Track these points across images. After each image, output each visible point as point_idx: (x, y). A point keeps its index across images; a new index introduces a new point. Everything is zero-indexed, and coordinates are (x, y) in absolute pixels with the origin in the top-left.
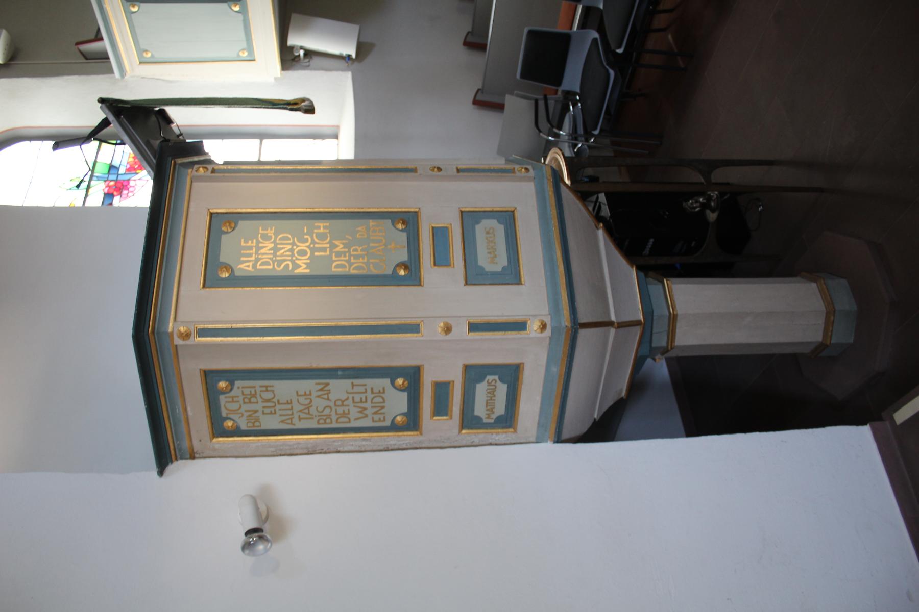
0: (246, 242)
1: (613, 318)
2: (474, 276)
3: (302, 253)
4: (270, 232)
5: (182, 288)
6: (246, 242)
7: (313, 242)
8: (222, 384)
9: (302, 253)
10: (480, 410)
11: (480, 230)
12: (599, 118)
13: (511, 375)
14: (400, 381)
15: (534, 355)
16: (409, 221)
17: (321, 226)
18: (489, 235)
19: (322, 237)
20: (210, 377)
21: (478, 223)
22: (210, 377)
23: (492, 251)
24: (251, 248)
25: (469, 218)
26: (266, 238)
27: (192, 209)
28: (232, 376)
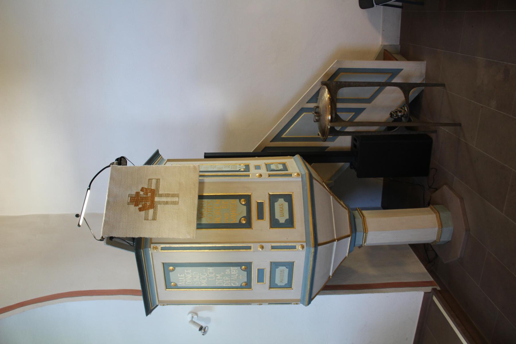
0: (180, 275)
1: (335, 238)
2: (274, 224)
3: (204, 279)
4: (190, 271)
5: (158, 290)
6: (180, 275)
7: (208, 275)
8: (171, 268)
9: (204, 279)
10: (278, 281)
11: (278, 271)
12: (334, 232)
13: (290, 265)
14: (243, 267)
15: (299, 257)
16: (247, 267)
17: (210, 269)
18: (281, 205)
19: (210, 273)
20: (165, 265)
21: (277, 268)
22: (165, 265)
23: (282, 211)
24: (182, 277)
25: (274, 265)
26: (188, 273)
27: (155, 263)
28: (176, 265)
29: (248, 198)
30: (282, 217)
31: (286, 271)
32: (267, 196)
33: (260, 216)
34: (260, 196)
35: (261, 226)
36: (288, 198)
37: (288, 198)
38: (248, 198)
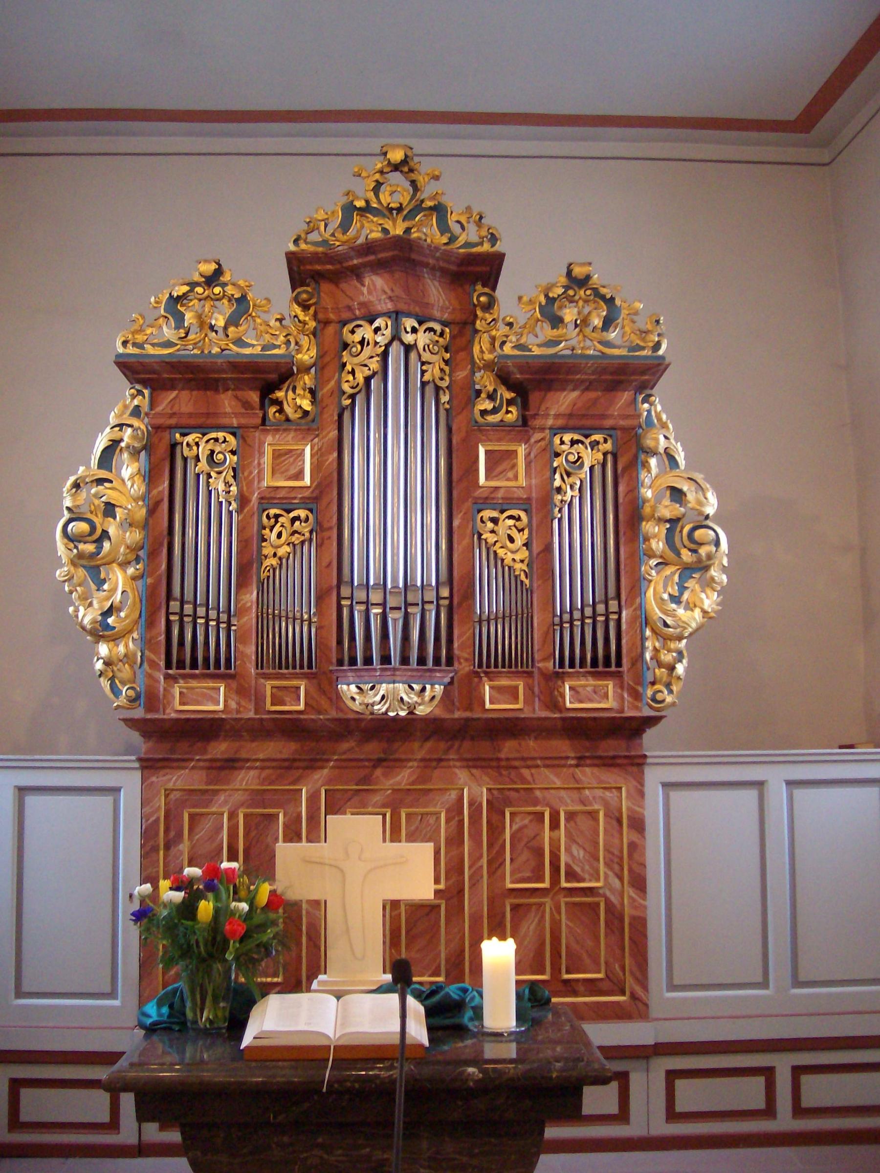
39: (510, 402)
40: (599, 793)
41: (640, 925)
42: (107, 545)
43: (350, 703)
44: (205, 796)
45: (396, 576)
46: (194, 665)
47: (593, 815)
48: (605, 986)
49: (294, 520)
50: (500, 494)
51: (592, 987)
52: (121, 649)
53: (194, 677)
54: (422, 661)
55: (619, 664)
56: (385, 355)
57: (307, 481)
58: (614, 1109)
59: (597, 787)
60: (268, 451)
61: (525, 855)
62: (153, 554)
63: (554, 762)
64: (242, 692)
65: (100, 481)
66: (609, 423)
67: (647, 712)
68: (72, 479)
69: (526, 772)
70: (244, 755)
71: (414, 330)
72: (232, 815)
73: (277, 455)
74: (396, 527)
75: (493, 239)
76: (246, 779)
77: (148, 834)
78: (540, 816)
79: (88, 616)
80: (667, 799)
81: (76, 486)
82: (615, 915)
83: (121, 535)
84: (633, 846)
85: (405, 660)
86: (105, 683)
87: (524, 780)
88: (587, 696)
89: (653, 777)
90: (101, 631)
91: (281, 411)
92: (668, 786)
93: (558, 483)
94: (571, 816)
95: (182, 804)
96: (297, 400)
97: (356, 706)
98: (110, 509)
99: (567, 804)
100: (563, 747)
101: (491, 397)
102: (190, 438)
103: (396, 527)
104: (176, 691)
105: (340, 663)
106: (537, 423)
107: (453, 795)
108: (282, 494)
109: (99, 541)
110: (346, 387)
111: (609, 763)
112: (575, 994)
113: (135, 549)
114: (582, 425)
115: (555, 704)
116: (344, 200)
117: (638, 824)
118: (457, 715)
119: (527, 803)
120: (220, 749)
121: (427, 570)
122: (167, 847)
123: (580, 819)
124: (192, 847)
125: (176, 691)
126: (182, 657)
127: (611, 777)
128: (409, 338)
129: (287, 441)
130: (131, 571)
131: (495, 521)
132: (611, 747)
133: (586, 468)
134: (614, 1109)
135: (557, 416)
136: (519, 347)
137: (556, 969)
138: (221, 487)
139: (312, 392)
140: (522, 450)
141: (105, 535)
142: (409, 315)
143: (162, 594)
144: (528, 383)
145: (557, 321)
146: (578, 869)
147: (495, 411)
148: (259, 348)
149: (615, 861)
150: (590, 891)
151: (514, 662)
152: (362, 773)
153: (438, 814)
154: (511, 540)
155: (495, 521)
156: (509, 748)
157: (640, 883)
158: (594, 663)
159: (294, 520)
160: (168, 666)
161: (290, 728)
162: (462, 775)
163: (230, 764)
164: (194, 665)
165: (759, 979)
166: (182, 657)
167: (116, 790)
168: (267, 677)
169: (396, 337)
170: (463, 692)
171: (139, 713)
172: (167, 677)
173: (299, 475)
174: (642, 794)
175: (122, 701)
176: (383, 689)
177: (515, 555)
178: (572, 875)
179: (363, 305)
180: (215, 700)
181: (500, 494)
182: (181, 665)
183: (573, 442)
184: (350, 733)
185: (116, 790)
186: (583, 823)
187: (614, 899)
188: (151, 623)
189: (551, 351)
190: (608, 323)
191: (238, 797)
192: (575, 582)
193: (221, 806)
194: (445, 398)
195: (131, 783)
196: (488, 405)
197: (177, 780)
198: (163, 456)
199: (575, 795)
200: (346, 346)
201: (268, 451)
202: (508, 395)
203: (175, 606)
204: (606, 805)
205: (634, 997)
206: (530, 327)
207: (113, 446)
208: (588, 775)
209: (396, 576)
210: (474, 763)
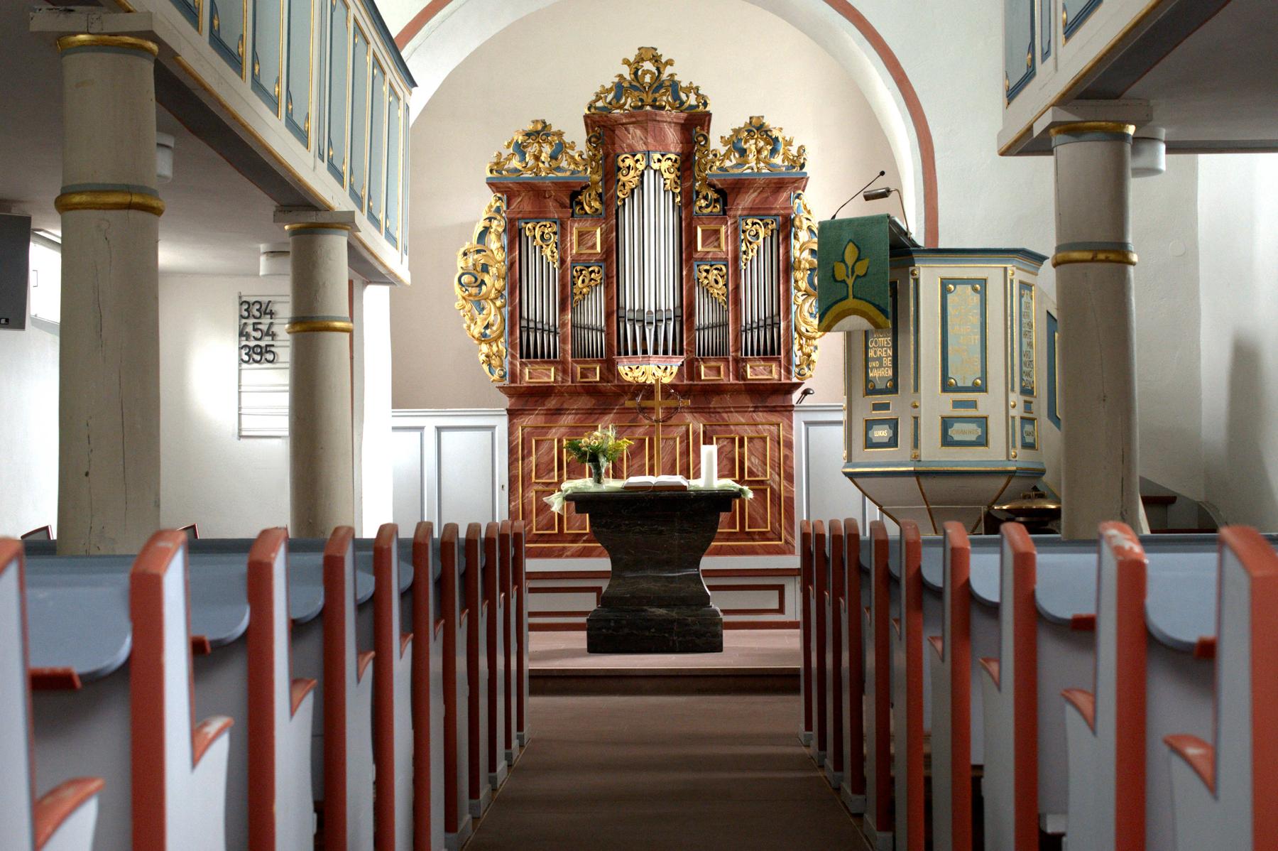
18: (881, 433)
23: (964, 432)
29: (894, 389)
30: (957, 432)
31: (973, 438)
32: (984, 414)
33: (973, 404)
34: (897, 406)
35: (865, 409)
36: (983, 441)
37: (983, 441)
38: (894, 389)
39: (716, 201)
40: (767, 427)
41: (790, 501)
42: (484, 288)
43: (625, 377)
44: (545, 429)
45: (650, 306)
46: (536, 356)
47: (764, 439)
48: (770, 536)
49: (591, 272)
50: (710, 256)
51: (763, 536)
52: (495, 349)
53: (537, 363)
54: (665, 352)
55: (779, 353)
56: (642, 175)
57: (599, 249)
58: (776, 606)
59: (765, 423)
60: (575, 231)
61: (725, 462)
62: (512, 293)
63: (741, 410)
64: (565, 372)
65: (478, 252)
66: (774, 212)
67: (795, 380)
68: (462, 250)
69: (725, 415)
70: (565, 406)
71: (659, 161)
72: (560, 441)
73: (581, 235)
74: (652, 281)
75: (705, 104)
76: (568, 420)
77: (512, 451)
78: (734, 439)
79: (477, 330)
80: (807, 431)
81: (465, 254)
82: (776, 497)
83: (492, 282)
84: (786, 457)
85: (656, 352)
86: (485, 367)
87: (723, 419)
88: (757, 372)
89: (798, 419)
90: (483, 338)
91: (583, 208)
92: (808, 424)
93: (744, 248)
94: (751, 439)
95: (531, 434)
96: (591, 204)
97: (629, 378)
98: (485, 268)
99: (748, 432)
100: (746, 401)
101: (705, 198)
102: (530, 225)
103: (652, 281)
104: (527, 371)
105: (619, 354)
106: (732, 213)
107: (684, 428)
108: (584, 257)
109: (480, 286)
110: (620, 194)
111: (773, 410)
112: (754, 540)
113: (500, 293)
114: (757, 212)
115: (740, 375)
116: (617, 80)
117: (789, 445)
118: (685, 382)
119: (726, 432)
120: (552, 403)
121: (668, 301)
122: (523, 459)
123: (756, 441)
124: (537, 459)
125: (527, 371)
126: (528, 353)
127: (774, 418)
128: (656, 166)
129: (586, 225)
130: (498, 303)
131: (707, 271)
132: (776, 401)
133: (761, 239)
134: (776, 606)
135: (743, 209)
136: (721, 169)
137: (742, 526)
138: (549, 253)
139: (600, 195)
140: (723, 229)
141: (483, 282)
142: (655, 151)
143: (515, 318)
144: (727, 192)
145: (743, 152)
146: (545, 522)
147: (707, 206)
148: (568, 173)
149: (776, 466)
150: (762, 482)
151: (719, 352)
152: (632, 416)
153: (675, 439)
154: (717, 282)
155: (707, 271)
156: (714, 403)
157: (790, 478)
158: (765, 353)
159: (591, 272)
160: (521, 357)
161: (591, 390)
162: (688, 417)
163: (558, 412)
164: (536, 356)
165: (444, 434)
166: (528, 353)
167: (493, 427)
168: (578, 362)
169: (648, 166)
170: (690, 369)
171: (507, 382)
172: (522, 364)
173: (594, 246)
174: (791, 427)
175: (496, 377)
176: (643, 368)
177: (718, 290)
178: (751, 473)
179: (629, 145)
180: (549, 376)
181: (710, 256)
182: (528, 356)
183: (754, 224)
184: (626, 393)
185: (493, 427)
186: (758, 444)
187: (775, 487)
188: (512, 332)
189: (740, 171)
190: (774, 152)
191: (563, 430)
192: (755, 305)
193: (554, 434)
194: (678, 199)
195: (502, 424)
196: (703, 203)
197: (529, 421)
198: (514, 235)
199: (753, 428)
200: (619, 169)
201: (575, 231)
202: (715, 196)
203: (524, 323)
204: (771, 433)
205: (786, 542)
206: (726, 156)
207: (486, 230)
208: (760, 417)
209: (650, 306)
210: (694, 410)
